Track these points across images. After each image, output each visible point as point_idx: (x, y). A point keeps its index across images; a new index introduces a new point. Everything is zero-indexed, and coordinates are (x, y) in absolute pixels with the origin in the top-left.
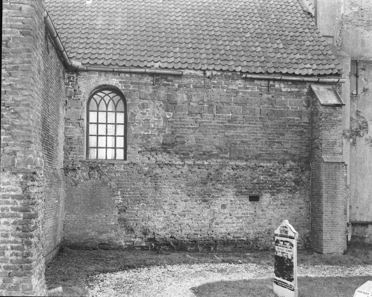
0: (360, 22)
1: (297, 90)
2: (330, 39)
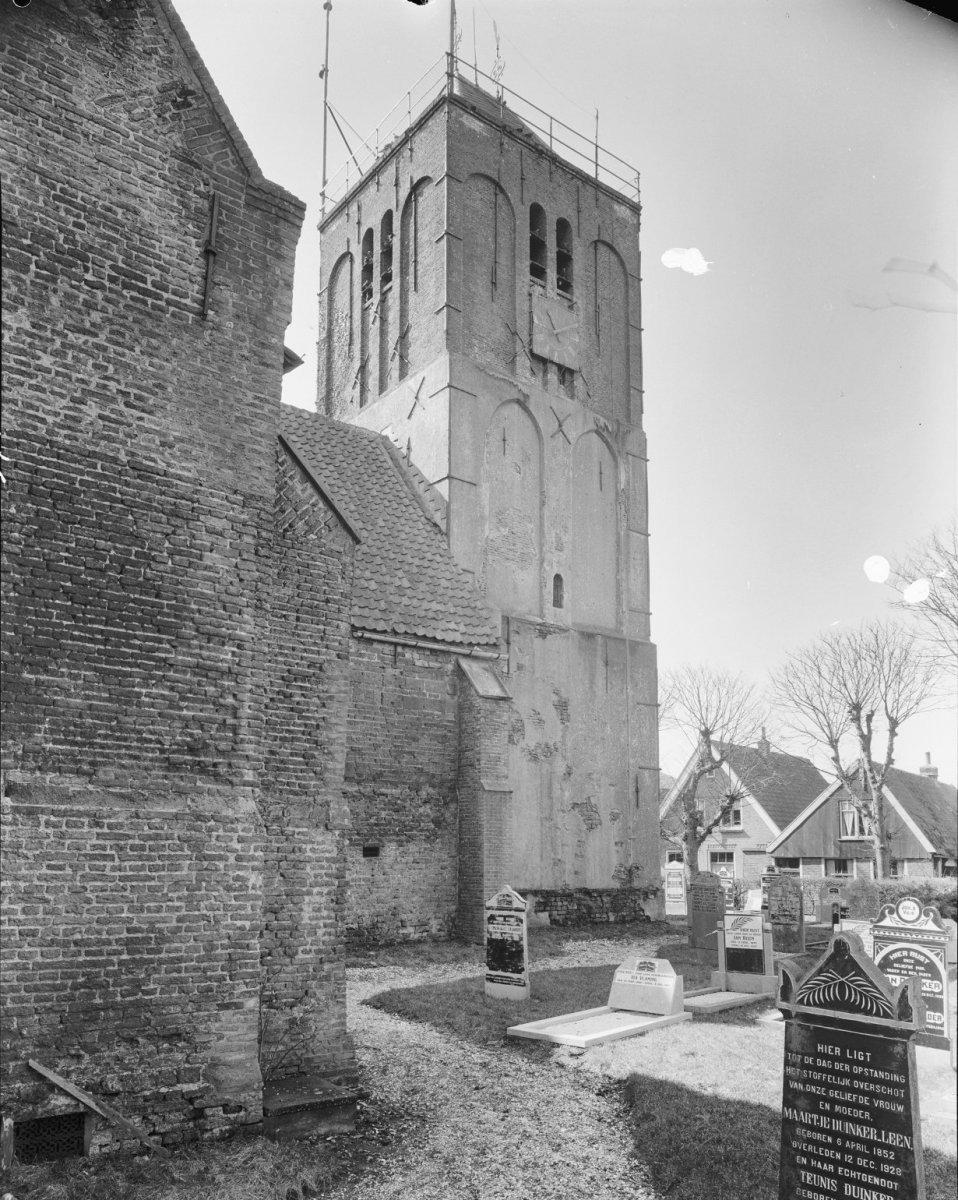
0: (511, 553)
1: (438, 665)
2: (470, 576)
